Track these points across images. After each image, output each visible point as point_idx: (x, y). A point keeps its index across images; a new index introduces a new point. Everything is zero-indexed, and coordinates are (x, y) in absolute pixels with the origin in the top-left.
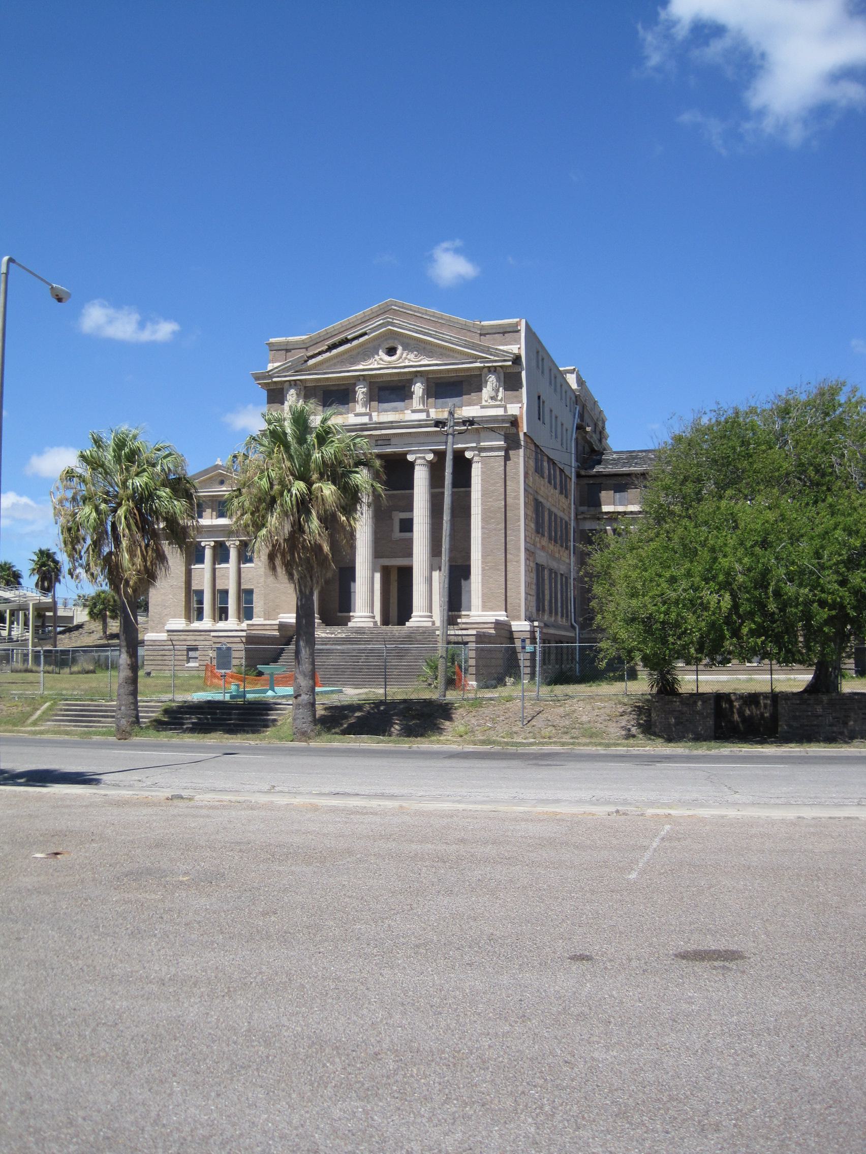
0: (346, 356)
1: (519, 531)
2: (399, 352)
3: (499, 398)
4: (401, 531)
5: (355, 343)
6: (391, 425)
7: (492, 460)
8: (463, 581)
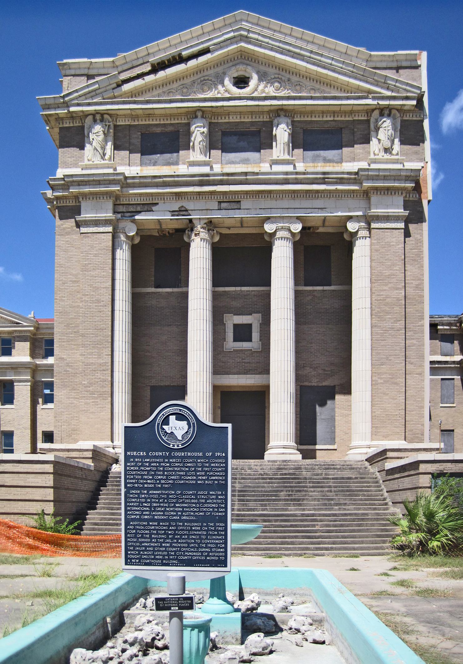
0: (175, 85)
1: (423, 332)
2: (253, 83)
3: (394, 152)
4: (235, 340)
5: (192, 63)
6: (244, 178)
7: (388, 233)
8: (318, 408)
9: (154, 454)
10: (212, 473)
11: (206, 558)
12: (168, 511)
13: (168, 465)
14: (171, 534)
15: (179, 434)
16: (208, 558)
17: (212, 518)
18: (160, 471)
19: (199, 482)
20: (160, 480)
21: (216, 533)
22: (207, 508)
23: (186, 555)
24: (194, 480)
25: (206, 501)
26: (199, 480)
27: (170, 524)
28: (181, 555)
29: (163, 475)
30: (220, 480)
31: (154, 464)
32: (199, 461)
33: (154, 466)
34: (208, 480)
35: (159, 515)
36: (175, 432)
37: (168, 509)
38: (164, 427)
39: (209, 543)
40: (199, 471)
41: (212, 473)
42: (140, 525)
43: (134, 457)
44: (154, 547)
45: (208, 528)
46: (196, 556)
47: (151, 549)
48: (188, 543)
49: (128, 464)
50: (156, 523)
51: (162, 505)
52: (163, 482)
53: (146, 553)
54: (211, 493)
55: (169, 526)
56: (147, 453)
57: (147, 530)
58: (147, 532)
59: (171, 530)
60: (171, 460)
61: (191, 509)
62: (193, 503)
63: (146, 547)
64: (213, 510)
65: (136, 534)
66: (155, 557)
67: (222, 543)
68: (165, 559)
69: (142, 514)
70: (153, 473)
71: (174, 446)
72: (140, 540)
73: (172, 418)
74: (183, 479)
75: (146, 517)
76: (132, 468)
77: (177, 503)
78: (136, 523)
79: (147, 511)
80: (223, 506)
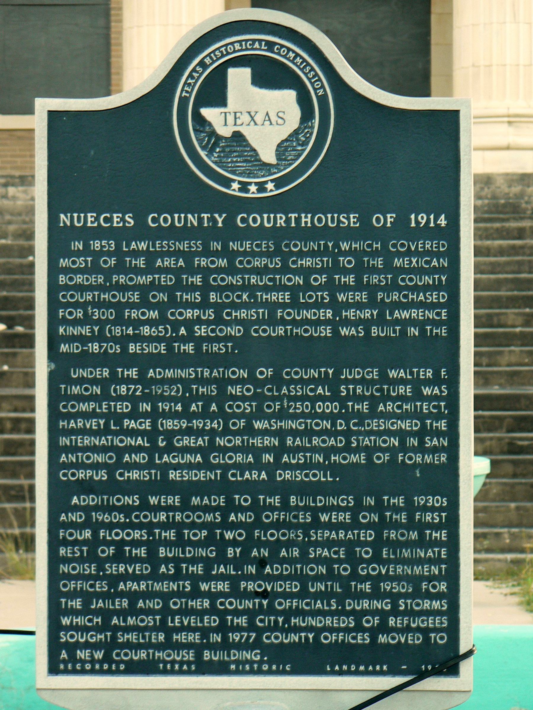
9: (165, 220)
10: (395, 296)
11: (374, 638)
12: (224, 450)
13: (223, 263)
14: (234, 543)
15: (265, 144)
16: (382, 639)
17: (397, 478)
18: (193, 288)
19: (344, 331)
20: (189, 324)
21: (414, 535)
22: (379, 434)
23: (296, 629)
24: (327, 322)
25: (373, 408)
26: (347, 323)
27: (230, 501)
28: (276, 627)
29: (204, 304)
30: (429, 322)
31: (169, 262)
32: (345, 246)
33: (167, 270)
34: (381, 321)
35: (190, 466)
36: (248, 132)
37: (220, 441)
38: (207, 112)
39: (387, 578)
40: (346, 288)
41: (395, 296)
42: (110, 509)
43: (87, 234)
44: (166, 597)
45: (382, 518)
46: (335, 629)
47: (156, 604)
48: (303, 579)
49: (63, 263)
50: (176, 500)
51: (197, 423)
52: (201, 331)
53: (131, 621)
54: (393, 374)
55: (225, 512)
56: (140, 219)
57: (140, 526)
58: (136, 535)
59: (233, 526)
60: (233, 246)
61: (316, 441)
62: (323, 416)
63: (133, 597)
64: (402, 442)
65: (95, 542)
66: (168, 638)
67: (439, 578)
68: (213, 647)
69: (119, 464)
70: (163, 297)
71: (244, 187)
72: (112, 569)
73: (239, 78)
74: (283, 322)
75: (135, 475)
76: (79, 279)
77: (260, 415)
78: (91, 500)
79: (139, 449)
80: (443, 425)
